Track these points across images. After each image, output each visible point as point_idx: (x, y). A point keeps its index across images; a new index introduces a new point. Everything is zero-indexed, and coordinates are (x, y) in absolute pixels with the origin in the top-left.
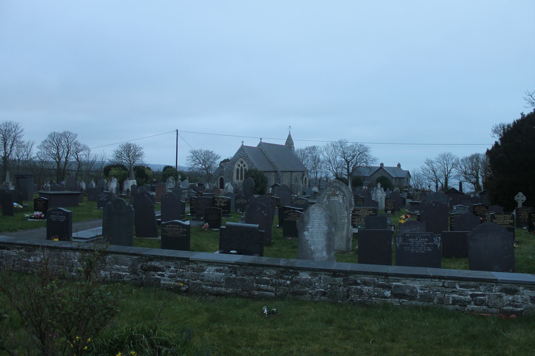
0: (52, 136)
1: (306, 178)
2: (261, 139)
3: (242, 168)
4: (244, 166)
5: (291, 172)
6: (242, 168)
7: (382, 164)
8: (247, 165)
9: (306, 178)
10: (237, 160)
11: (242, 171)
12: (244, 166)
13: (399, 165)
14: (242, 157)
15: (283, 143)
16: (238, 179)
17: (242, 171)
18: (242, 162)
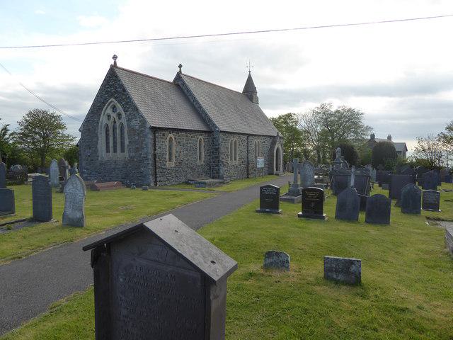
0: (30, 114)
1: (278, 149)
2: (180, 66)
3: (115, 122)
4: (119, 116)
5: (249, 135)
6: (115, 122)
7: (373, 136)
8: (123, 115)
9: (278, 149)
10: (104, 103)
11: (114, 129)
12: (119, 116)
13: (390, 138)
14: (112, 96)
15: (239, 87)
16: (108, 151)
17: (114, 129)
18: (114, 108)
